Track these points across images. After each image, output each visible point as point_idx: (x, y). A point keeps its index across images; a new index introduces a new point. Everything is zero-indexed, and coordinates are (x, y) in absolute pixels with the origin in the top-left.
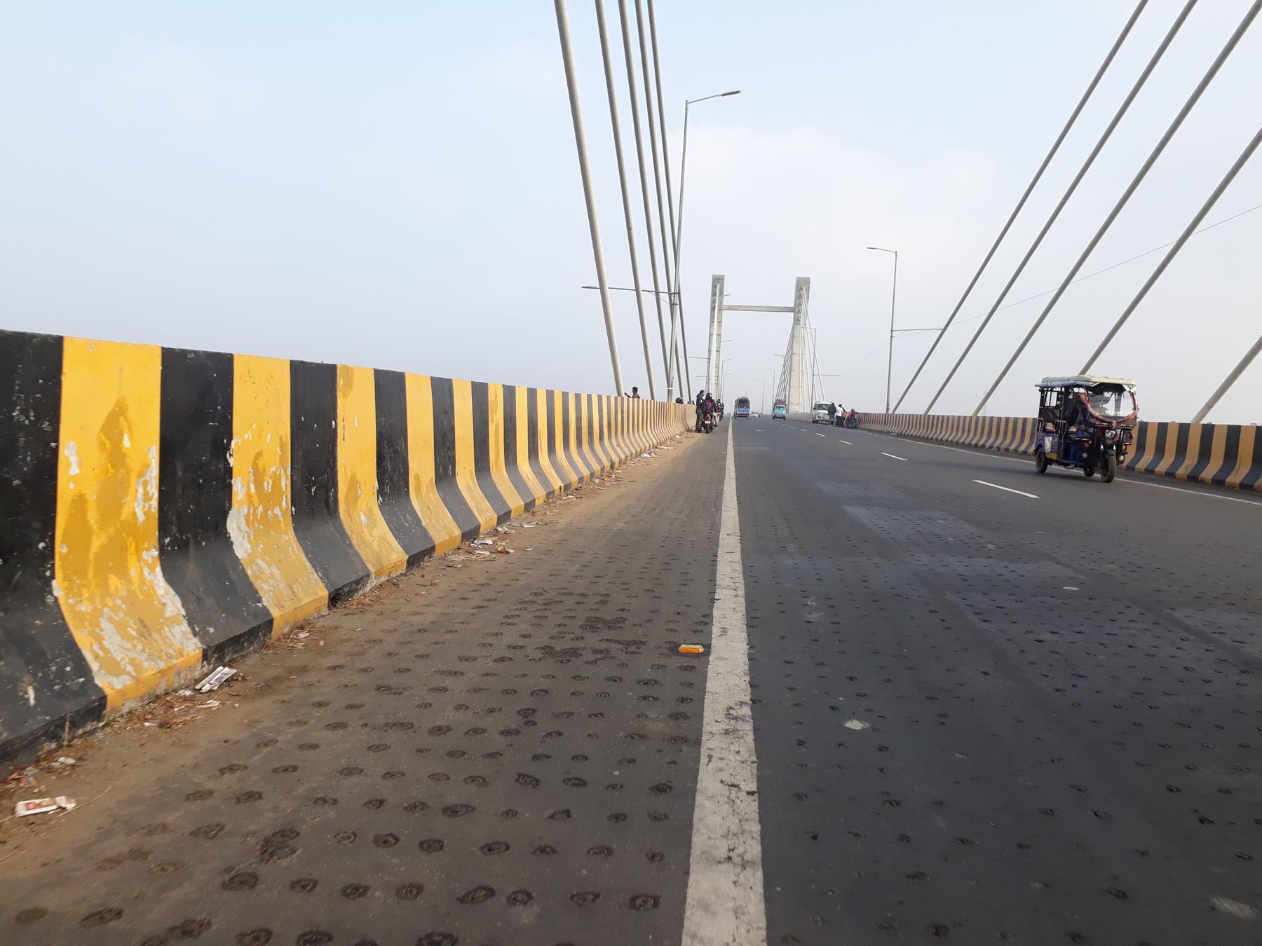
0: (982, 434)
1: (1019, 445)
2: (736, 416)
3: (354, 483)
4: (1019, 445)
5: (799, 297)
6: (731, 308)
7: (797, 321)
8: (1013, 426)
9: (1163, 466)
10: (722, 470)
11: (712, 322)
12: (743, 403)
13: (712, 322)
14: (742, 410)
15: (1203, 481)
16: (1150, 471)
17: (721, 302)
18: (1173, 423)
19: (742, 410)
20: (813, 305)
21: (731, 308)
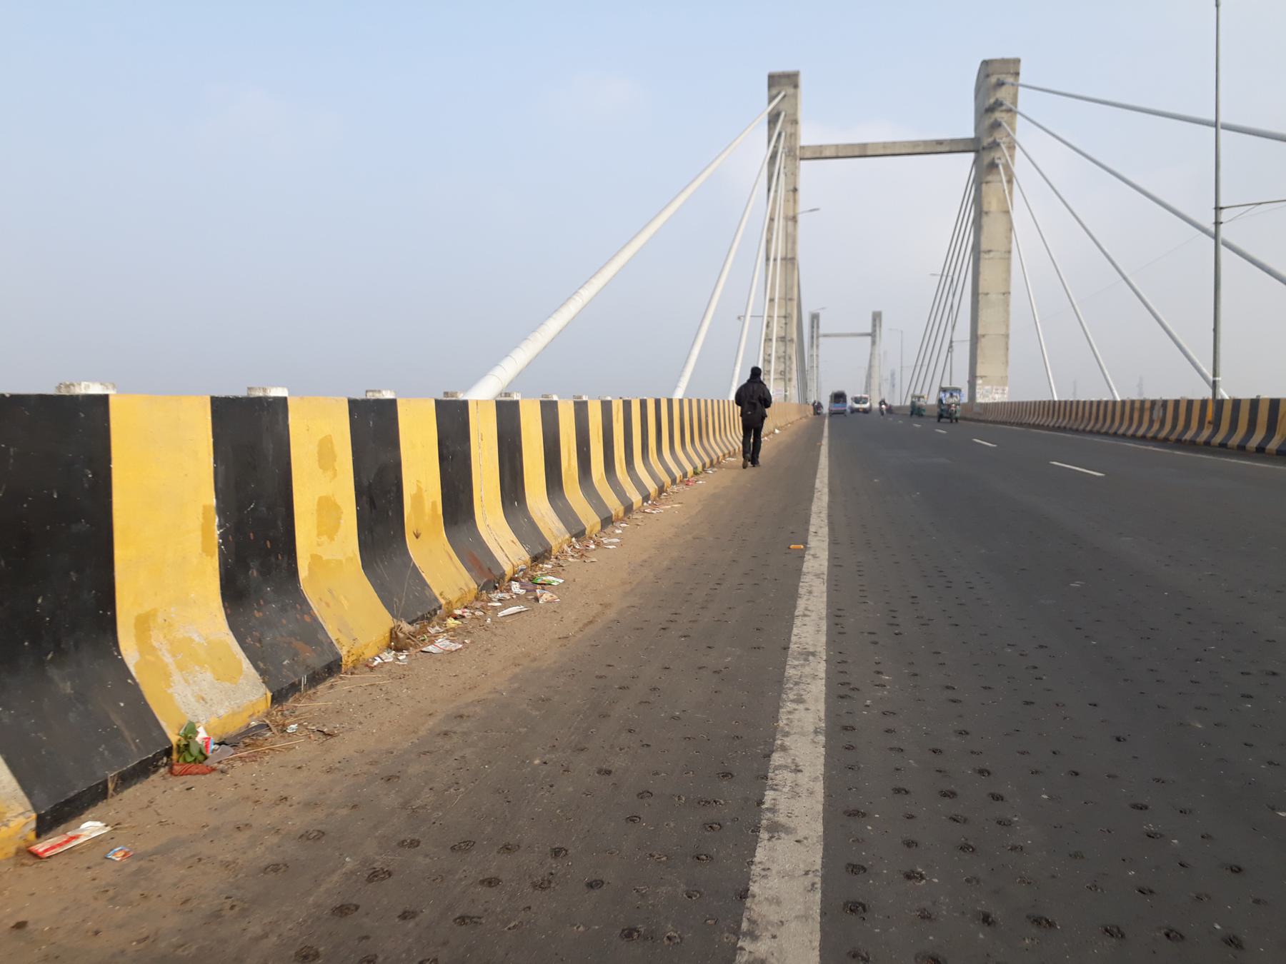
0: (1131, 419)
1: (1137, 430)
2: (832, 413)
3: (418, 498)
4: (1137, 430)
5: (874, 326)
6: (825, 336)
7: (874, 343)
8: (932, 406)
9: (1235, 440)
10: (822, 432)
11: (769, 190)
12: (839, 397)
13: (769, 190)
14: (838, 407)
15: (1232, 448)
16: (1242, 448)
17: (793, 136)
18: (1246, 400)
19: (838, 407)
20: (1032, 145)
21: (825, 336)
